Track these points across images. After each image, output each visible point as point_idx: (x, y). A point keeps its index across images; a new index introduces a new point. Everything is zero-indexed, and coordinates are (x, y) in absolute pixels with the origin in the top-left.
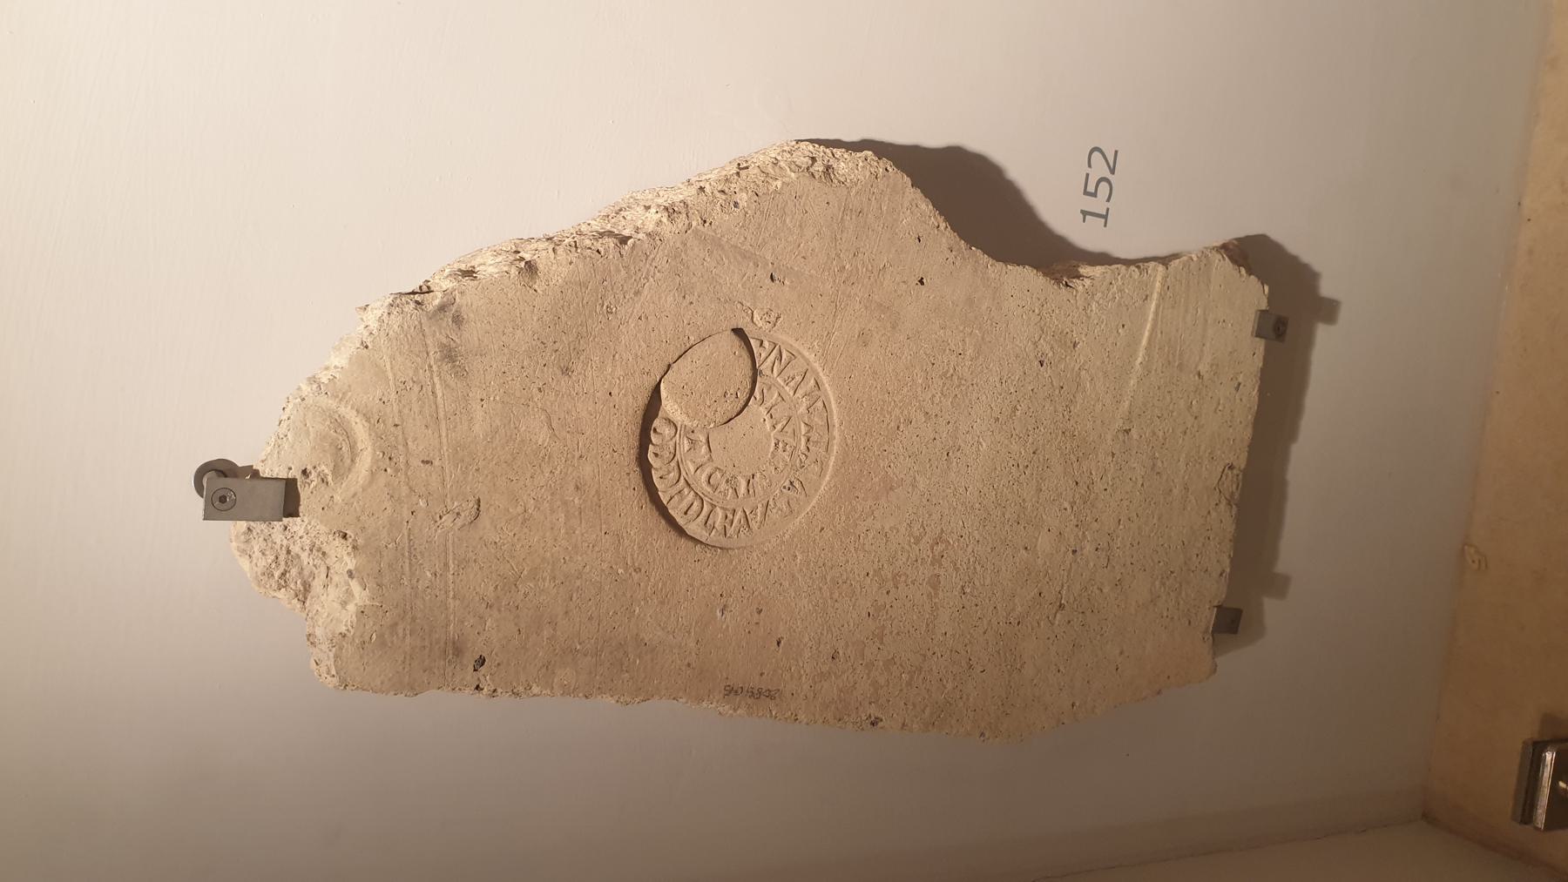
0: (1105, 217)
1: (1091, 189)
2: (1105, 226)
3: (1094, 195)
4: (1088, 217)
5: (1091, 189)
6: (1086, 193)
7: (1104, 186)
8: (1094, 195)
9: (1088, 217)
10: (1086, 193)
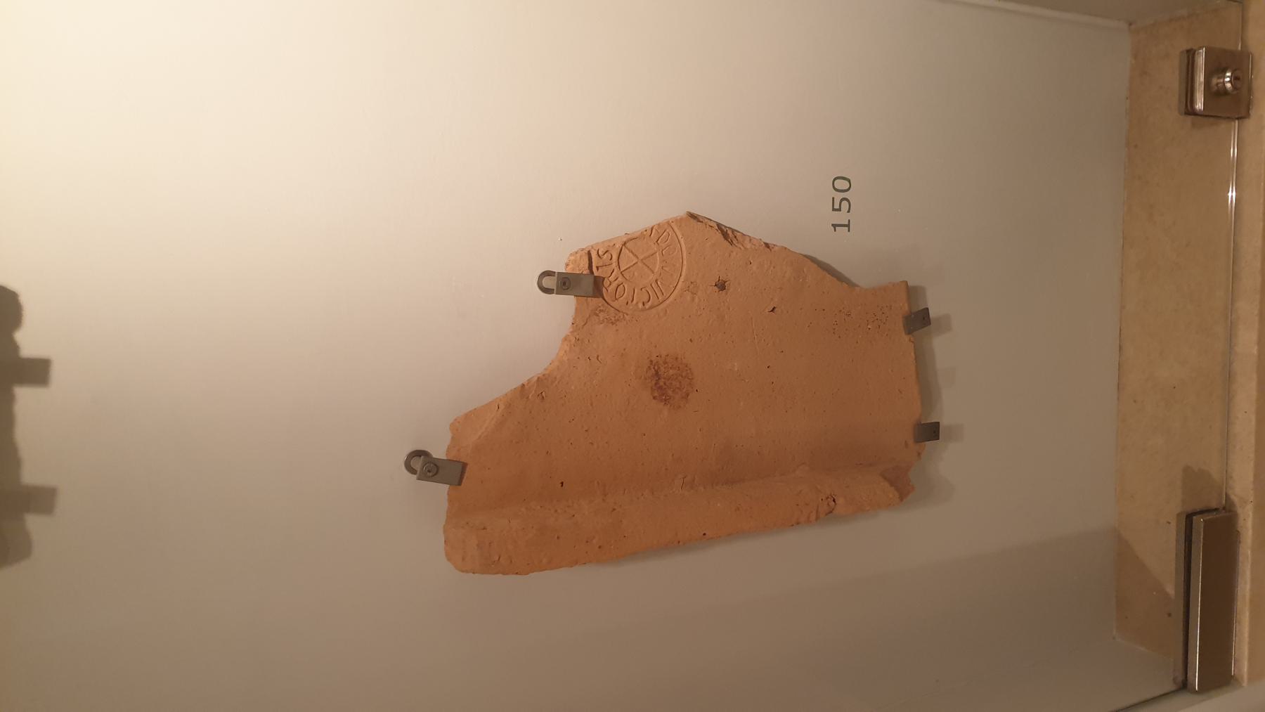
0: (848, 226)
1: (837, 206)
2: (849, 231)
3: (839, 210)
4: (837, 228)
5: (837, 206)
6: (834, 210)
7: (845, 204)
8: (839, 210)
9: (837, 228)
10: (834, 210)
